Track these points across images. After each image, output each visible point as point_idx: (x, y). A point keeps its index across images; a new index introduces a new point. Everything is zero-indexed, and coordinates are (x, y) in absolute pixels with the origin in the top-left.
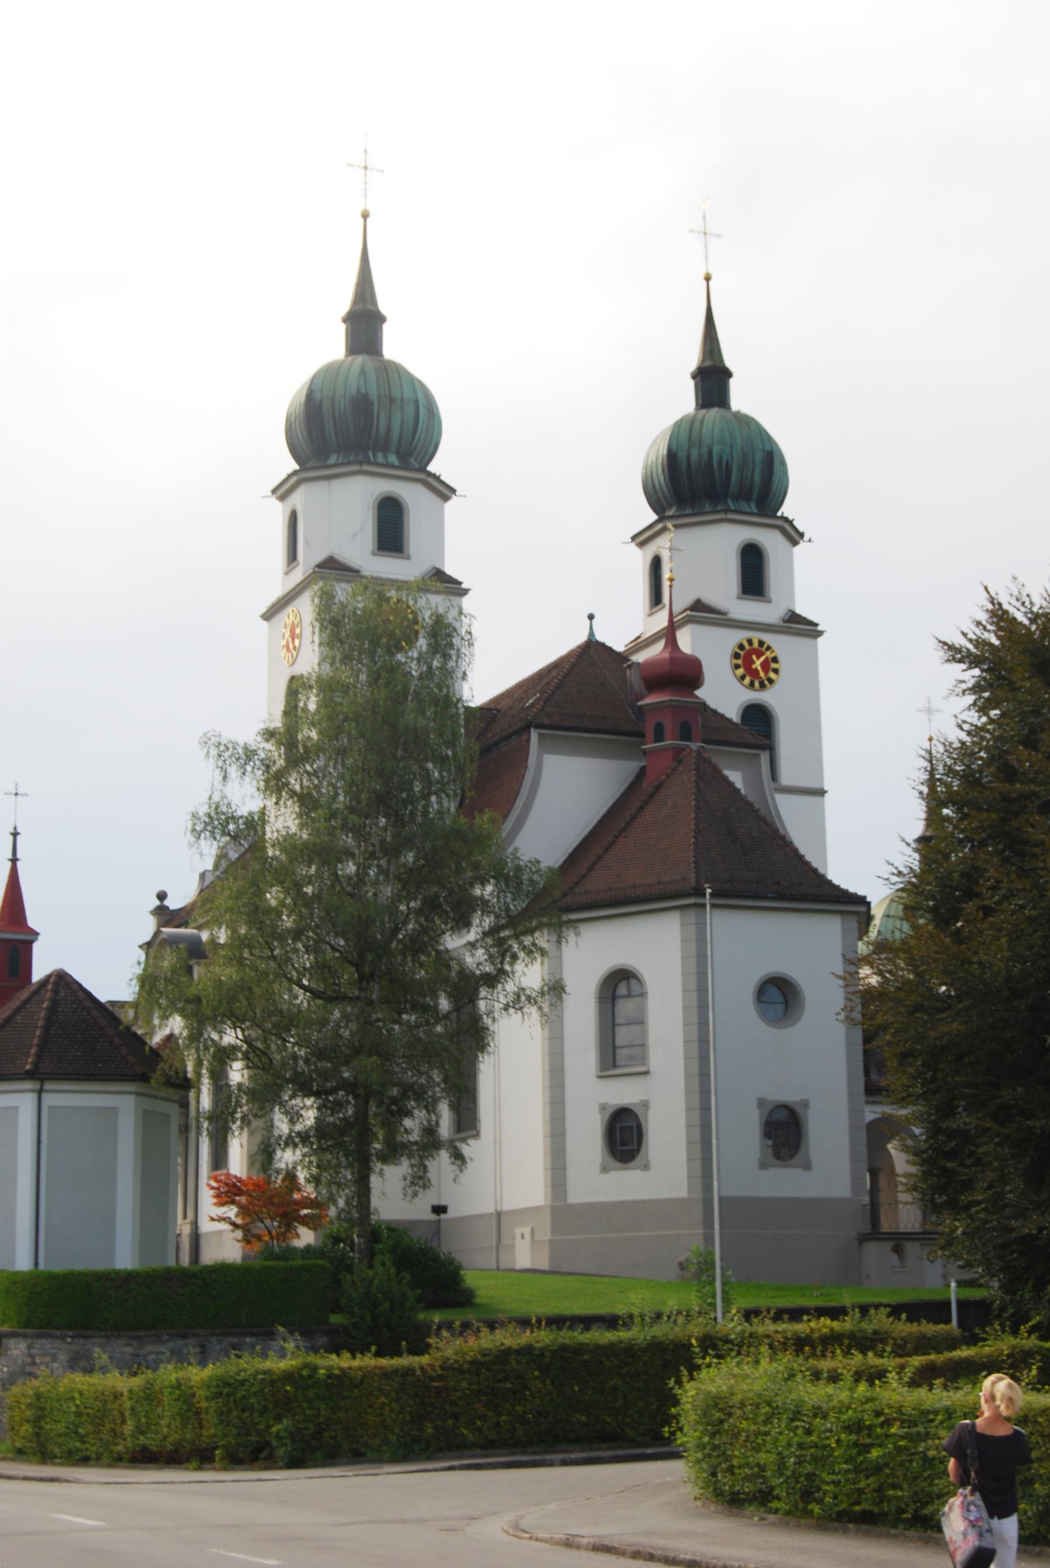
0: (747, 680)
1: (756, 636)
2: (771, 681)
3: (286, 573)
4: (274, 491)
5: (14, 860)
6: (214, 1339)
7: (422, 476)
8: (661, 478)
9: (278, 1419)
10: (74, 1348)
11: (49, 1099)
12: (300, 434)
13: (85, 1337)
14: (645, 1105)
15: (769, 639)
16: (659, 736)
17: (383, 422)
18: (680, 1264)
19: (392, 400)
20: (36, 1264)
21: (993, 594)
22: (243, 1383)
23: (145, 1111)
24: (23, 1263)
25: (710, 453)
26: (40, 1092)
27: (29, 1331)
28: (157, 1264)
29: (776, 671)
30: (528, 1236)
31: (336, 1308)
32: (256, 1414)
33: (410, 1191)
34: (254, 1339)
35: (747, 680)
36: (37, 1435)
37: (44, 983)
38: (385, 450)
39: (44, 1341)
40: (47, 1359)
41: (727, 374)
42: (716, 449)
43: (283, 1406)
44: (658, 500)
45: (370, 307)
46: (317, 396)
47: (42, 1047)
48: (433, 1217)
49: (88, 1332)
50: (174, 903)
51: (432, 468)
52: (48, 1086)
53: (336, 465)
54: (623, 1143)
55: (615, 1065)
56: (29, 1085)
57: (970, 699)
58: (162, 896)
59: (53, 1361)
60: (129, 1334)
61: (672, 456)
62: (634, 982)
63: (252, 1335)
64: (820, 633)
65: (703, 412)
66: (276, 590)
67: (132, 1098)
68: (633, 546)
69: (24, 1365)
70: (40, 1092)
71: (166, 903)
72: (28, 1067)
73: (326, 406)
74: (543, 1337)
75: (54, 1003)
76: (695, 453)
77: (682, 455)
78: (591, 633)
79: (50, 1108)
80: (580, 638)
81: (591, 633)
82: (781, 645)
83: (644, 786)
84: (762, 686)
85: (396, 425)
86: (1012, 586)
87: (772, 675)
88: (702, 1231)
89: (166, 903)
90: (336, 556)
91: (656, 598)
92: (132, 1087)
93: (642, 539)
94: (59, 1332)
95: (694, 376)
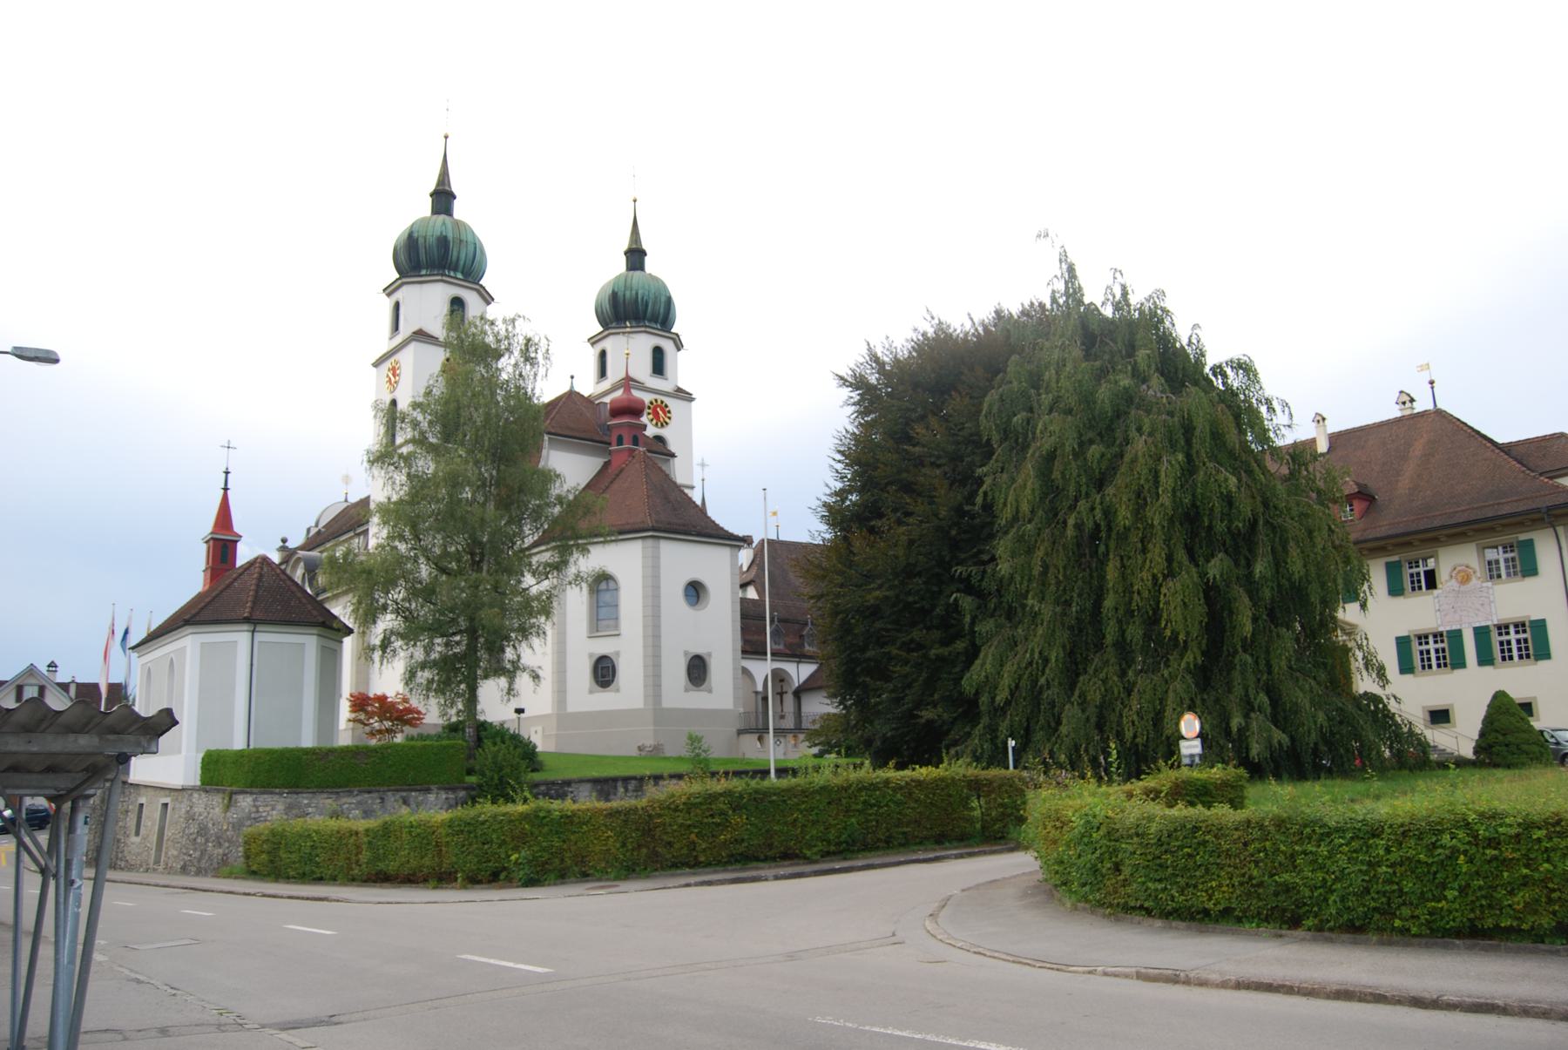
0: (654, 422)
1: (660, 398)
2: (667, 423)
3: (391, 339)
4: (384, 290)
5: (226, 489)
6: (390, 794)
7: (477, 287)
8: (606, 306)
9: (516, 849)
10: (288, 800)
11: (259, 637)
12: (402, 257)
13: (297, 793)
14: (618, 654)
15: (667, 400)
16: (620, 442)
17: (455, 254)
18: (639, 747)
19: (461, 241)
20: (248, 745)
21: (872, 346)
22: (483, 823)
23: (323, 647)
24: (239, 744)
25: (637, 294)
26: (253, 632)
27: (254, 790)
28: (326, 745)
29: (669, 418)
30: (540, 732)
31: (470, 772)
32: (495, 846)
33: (506, 698)
34: (418, 793)
35: (654, 422)
36: (272, 862)
37: (251, 564)
38: (455, 270)
39: (266, 796)
40: (268, 808)
41: (644, 253)
42: (640, 292)
43: (521, 840)
44: (605, 320)
45: (447, 188)
46: (416, 235)
47: (254, 603)
48: (515, 716)
49: (300, 790)
50: (291, 544)
51: (481, 283)
52: (259, 628)
53: (426, 275)
54: (603, 676)
55: (597, 631)
56: (245, 627)
57: (853, 408)
58: (284, 541)
59: (273, 809)
60: (329, 790)
61: (614, 295)
62: (611, 584)
63: (416, 790)
64: (693, 399)
65: (631, 272)
66: (385, 346)
67: (315, 637)
68: (589, 345)
69: (250, 813)
70: (253, 632)
71: (287, 544)
72: (246, 615)
73: (421, 241)
74: (737, 784)
75: (261, 576)
76: (628, 293)
77: (620, 294)
78: (572, 386)
79: (260, 642)
80: (564, 389)
81: (572, 386)
82: (673, 404)
83: (610, 471)
84: (662, 425)
85: (463, 256)
86: (885, 342)
87: (667, 420)
88: (652, 728)
89: (287, 544)
90: (424, 329)
91: (603, 373)
92: (315, 631)
93: (594, 341)
94: (277, 790)
95: (626, 253)
